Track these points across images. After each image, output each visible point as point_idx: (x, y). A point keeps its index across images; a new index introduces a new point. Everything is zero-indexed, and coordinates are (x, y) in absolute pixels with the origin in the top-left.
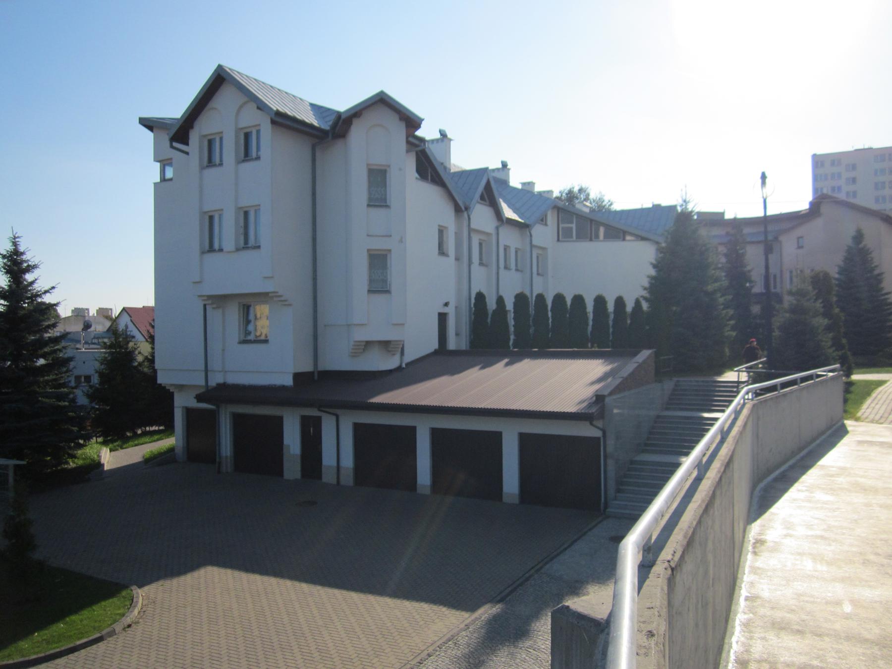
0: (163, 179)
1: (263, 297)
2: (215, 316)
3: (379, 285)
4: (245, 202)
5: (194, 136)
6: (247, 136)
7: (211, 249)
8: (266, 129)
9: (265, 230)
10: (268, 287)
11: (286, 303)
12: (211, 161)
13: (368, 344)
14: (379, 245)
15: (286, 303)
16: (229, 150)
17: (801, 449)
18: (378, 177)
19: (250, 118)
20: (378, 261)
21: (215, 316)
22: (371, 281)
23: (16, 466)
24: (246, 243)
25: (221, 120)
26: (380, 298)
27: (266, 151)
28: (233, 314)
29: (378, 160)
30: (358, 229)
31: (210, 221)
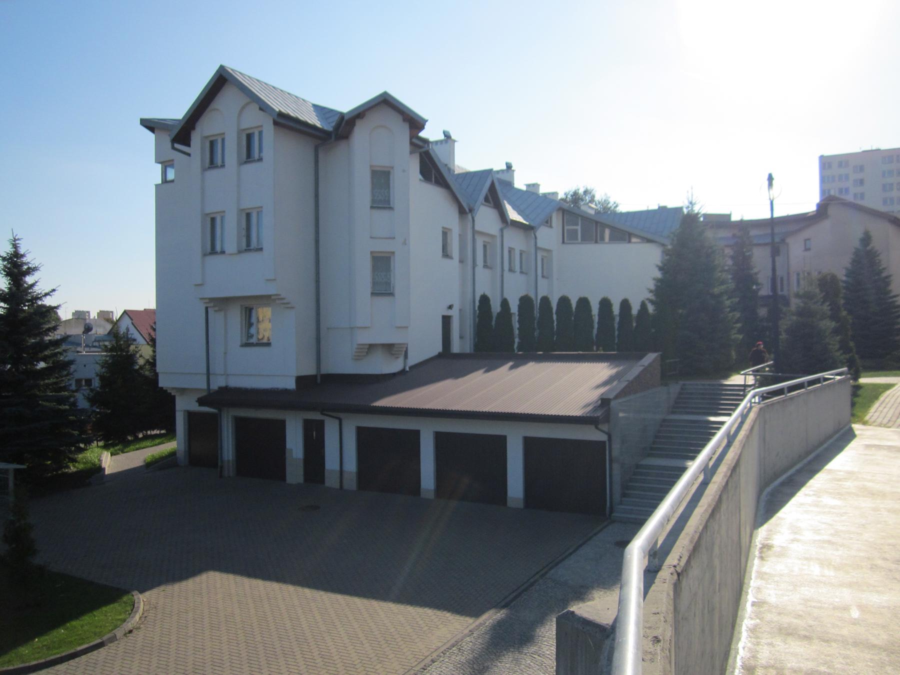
0: (165, 181)
1: (265, 299)
2: (217, 319)
3: (383, 288)
4: (247, 204)
5: (196, 138)
6: (249, 137)
7: (213, 252)
8: (269, 130)
9: (268, 232)
10: (271, 290)
11: (288, 306)
12: (212, 162)
13: (371, 347)
14: (382, 247)
15: (288, 306)
16: (231, 151)
17: (808, 453)
18: (381, 178)
19: (253, 119)
20: (382, 263)
21: (217, 319)
22: (374, 283)
23: (16, 470)
24: (249, 246)
25: (223, 121)
26: (384, 301)
27: (268, 153)
28: (235, 317)
29: (382, 162)
30: (361, 231)
31: (212, 223)
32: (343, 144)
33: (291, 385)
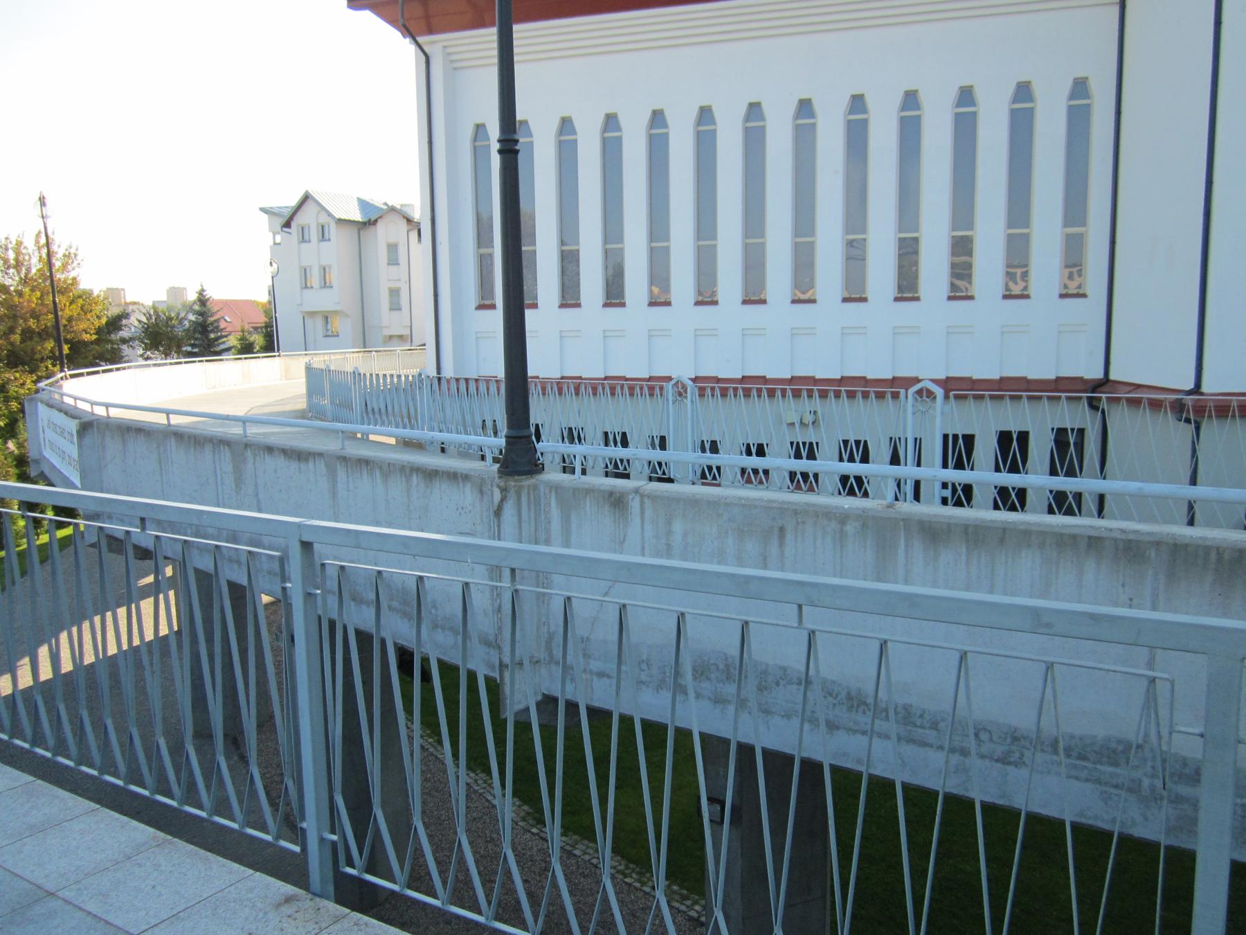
0: (275, 244)
1: (336, 312)
2: (309, 322)
3: (395, 307)
4: (324, 263)
5: (293, 224)
6: (323, 227)
7: (306, 287)
8: (333, 226)
9: (334, 277)
10: (338, 308)
11: (347, 316)
12: (303, 240)
13: (391, 337)
14: (394, 285)
15: (347, 316)
16: (314, 234)
17: (431, 475)
18: (392, 248)
19: (323, 219)
20: (394, 293)
21: (309, 322)
22: (391, 303)
23: (548, 542)
24: (325, 285)
25: (307, 217)
26: (395, 313)
27: (333, 237)
28: (320, 322)
29: (392, 240)
30: (384, 277)
31: (305, 272)
32: (372, 228)
33: (503, 717)
